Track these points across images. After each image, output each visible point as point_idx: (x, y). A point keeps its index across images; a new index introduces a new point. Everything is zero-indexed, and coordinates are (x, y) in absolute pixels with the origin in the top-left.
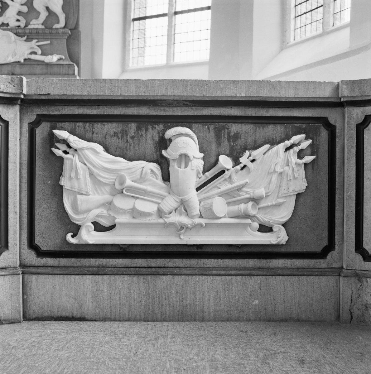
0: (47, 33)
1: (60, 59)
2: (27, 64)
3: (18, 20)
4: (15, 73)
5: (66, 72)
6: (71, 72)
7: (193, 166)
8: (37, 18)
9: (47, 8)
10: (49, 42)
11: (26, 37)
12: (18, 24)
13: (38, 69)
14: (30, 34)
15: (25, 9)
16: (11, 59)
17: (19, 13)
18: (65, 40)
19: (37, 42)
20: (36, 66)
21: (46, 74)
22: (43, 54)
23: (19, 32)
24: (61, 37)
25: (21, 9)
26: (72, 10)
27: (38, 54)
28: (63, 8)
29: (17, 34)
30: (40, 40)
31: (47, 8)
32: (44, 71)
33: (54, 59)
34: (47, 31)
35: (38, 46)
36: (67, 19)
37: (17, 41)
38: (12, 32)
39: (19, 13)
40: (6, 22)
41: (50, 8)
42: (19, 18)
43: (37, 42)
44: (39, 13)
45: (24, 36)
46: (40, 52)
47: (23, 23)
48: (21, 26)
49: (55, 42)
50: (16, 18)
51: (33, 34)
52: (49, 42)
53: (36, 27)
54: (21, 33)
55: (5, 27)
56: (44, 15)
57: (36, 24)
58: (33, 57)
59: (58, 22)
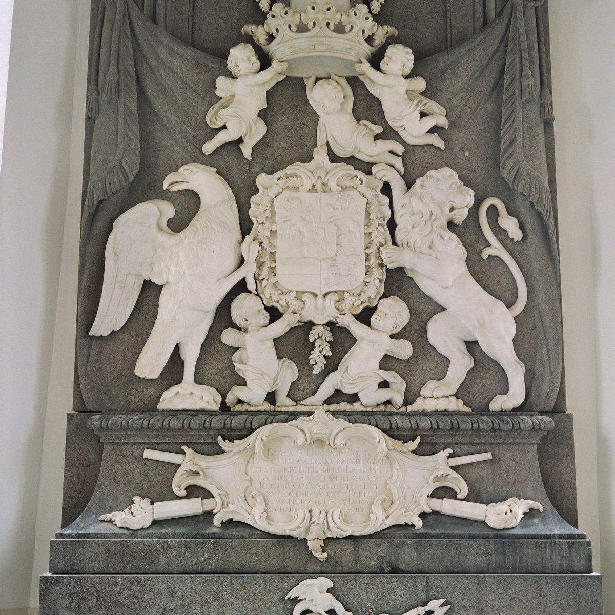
0: (483, 430)
1: (530, 514)
2: (438, 536)
3: (384, 385)
4: (402, 566)
5: (565, 563)
6: (579, 564)
7: (427, 577)
8: (441, 376)
9: (472, 346)
10: (488, 456)
11: (418, 439)
12: (384, 395)
13: (474, 554)
14: (431, 433)
15: (404, 349)
16: (378, 521)
17: (387, 362)
18: (535, 448)
19: (450, 456)
20: (465, 542)
21: (499, 570)
22: (474, 496)
23: (406, 428)
24: (526, 441)
25: (392, 349)
26: (544, 352)
27: (458, 496)
28: (517, 343)
29: (392, 433)
30: (458, 449)
31: (472, 346)
32: (494, 559)
33: (504, 514)
34: (487, 422)
35: (453, 468)
36: (530, 378)
37: (395, 455)
38: (377, 427)
39: (387, 362)
40: (348, 390)
41: (483, 346)
42: (387, 375)
43: (450, 456)
44: (447, 361)
45: (414, 439)
46: (463, 489)
47: (399, 392)
48: (392, 402)
49: (506, 455)
50: (383, 378)
51: (438, 433)
52: (488, 456)
53: (442, 405)
54: (404, 430)
55: (344, 406)
56: (460, 366)
57: (438, 396)
58: (447, 506)
59: (505, 392)
